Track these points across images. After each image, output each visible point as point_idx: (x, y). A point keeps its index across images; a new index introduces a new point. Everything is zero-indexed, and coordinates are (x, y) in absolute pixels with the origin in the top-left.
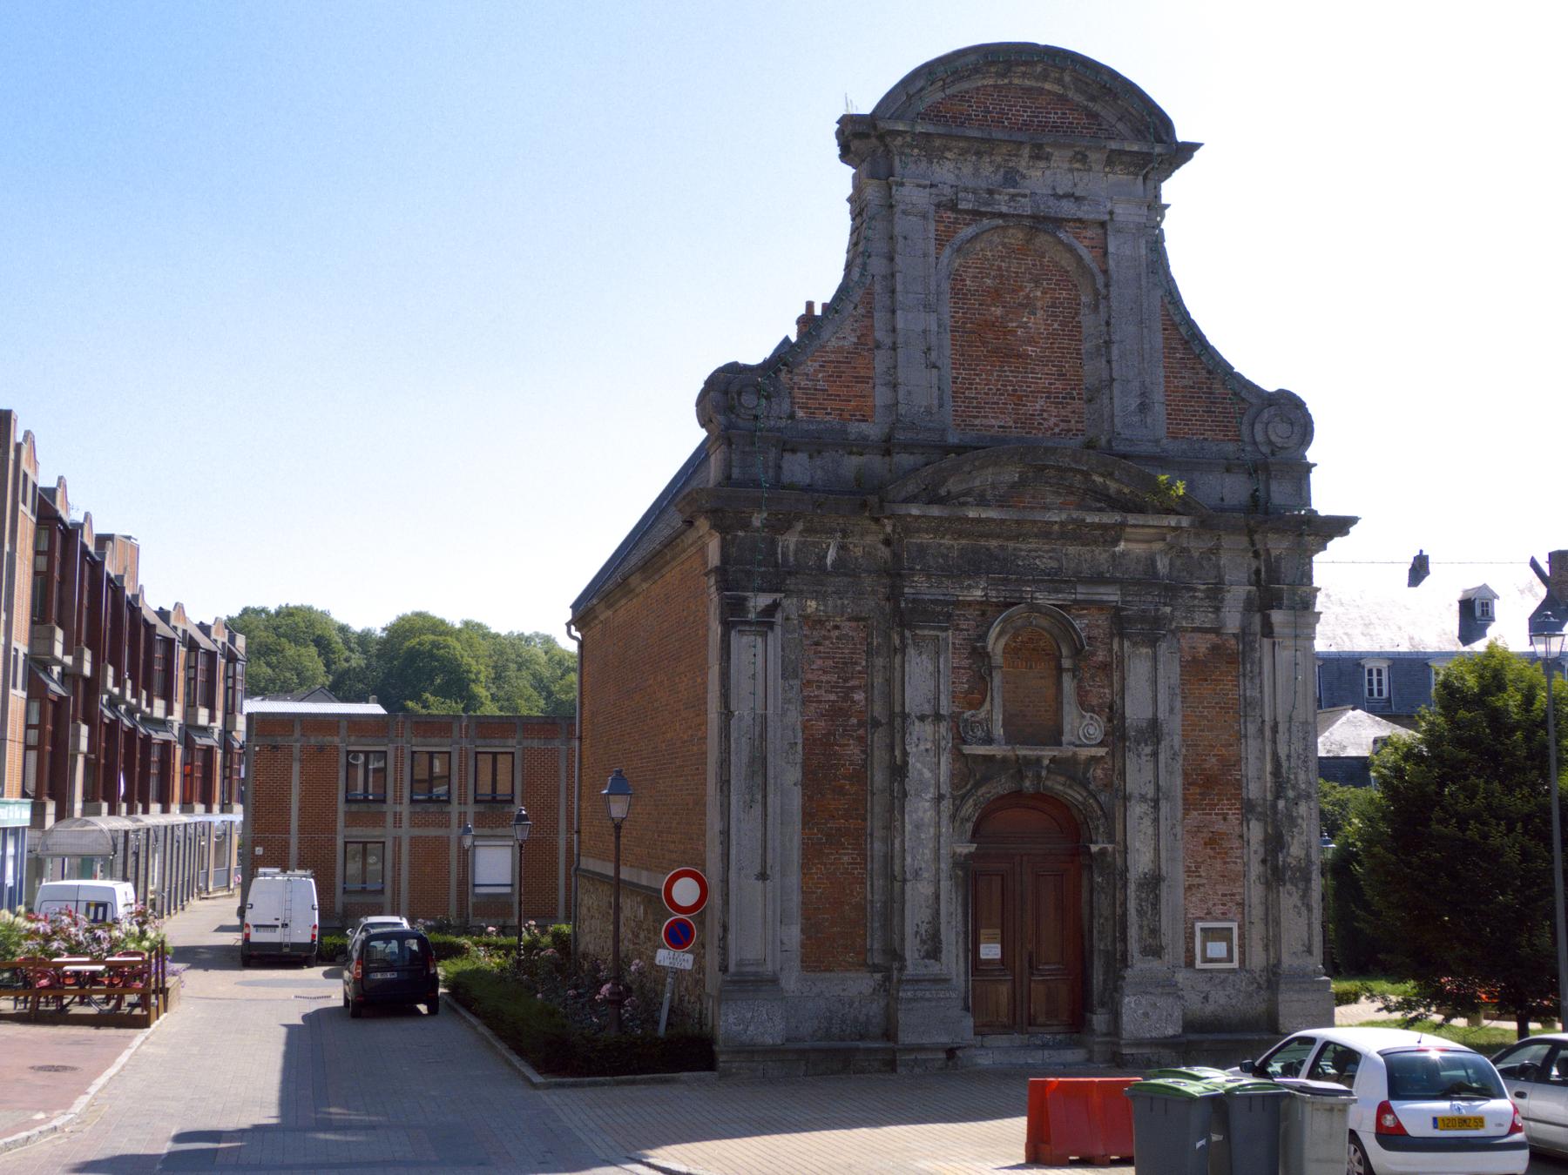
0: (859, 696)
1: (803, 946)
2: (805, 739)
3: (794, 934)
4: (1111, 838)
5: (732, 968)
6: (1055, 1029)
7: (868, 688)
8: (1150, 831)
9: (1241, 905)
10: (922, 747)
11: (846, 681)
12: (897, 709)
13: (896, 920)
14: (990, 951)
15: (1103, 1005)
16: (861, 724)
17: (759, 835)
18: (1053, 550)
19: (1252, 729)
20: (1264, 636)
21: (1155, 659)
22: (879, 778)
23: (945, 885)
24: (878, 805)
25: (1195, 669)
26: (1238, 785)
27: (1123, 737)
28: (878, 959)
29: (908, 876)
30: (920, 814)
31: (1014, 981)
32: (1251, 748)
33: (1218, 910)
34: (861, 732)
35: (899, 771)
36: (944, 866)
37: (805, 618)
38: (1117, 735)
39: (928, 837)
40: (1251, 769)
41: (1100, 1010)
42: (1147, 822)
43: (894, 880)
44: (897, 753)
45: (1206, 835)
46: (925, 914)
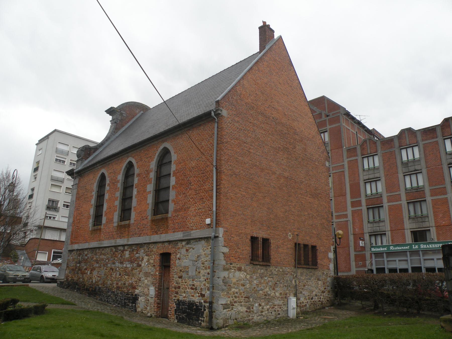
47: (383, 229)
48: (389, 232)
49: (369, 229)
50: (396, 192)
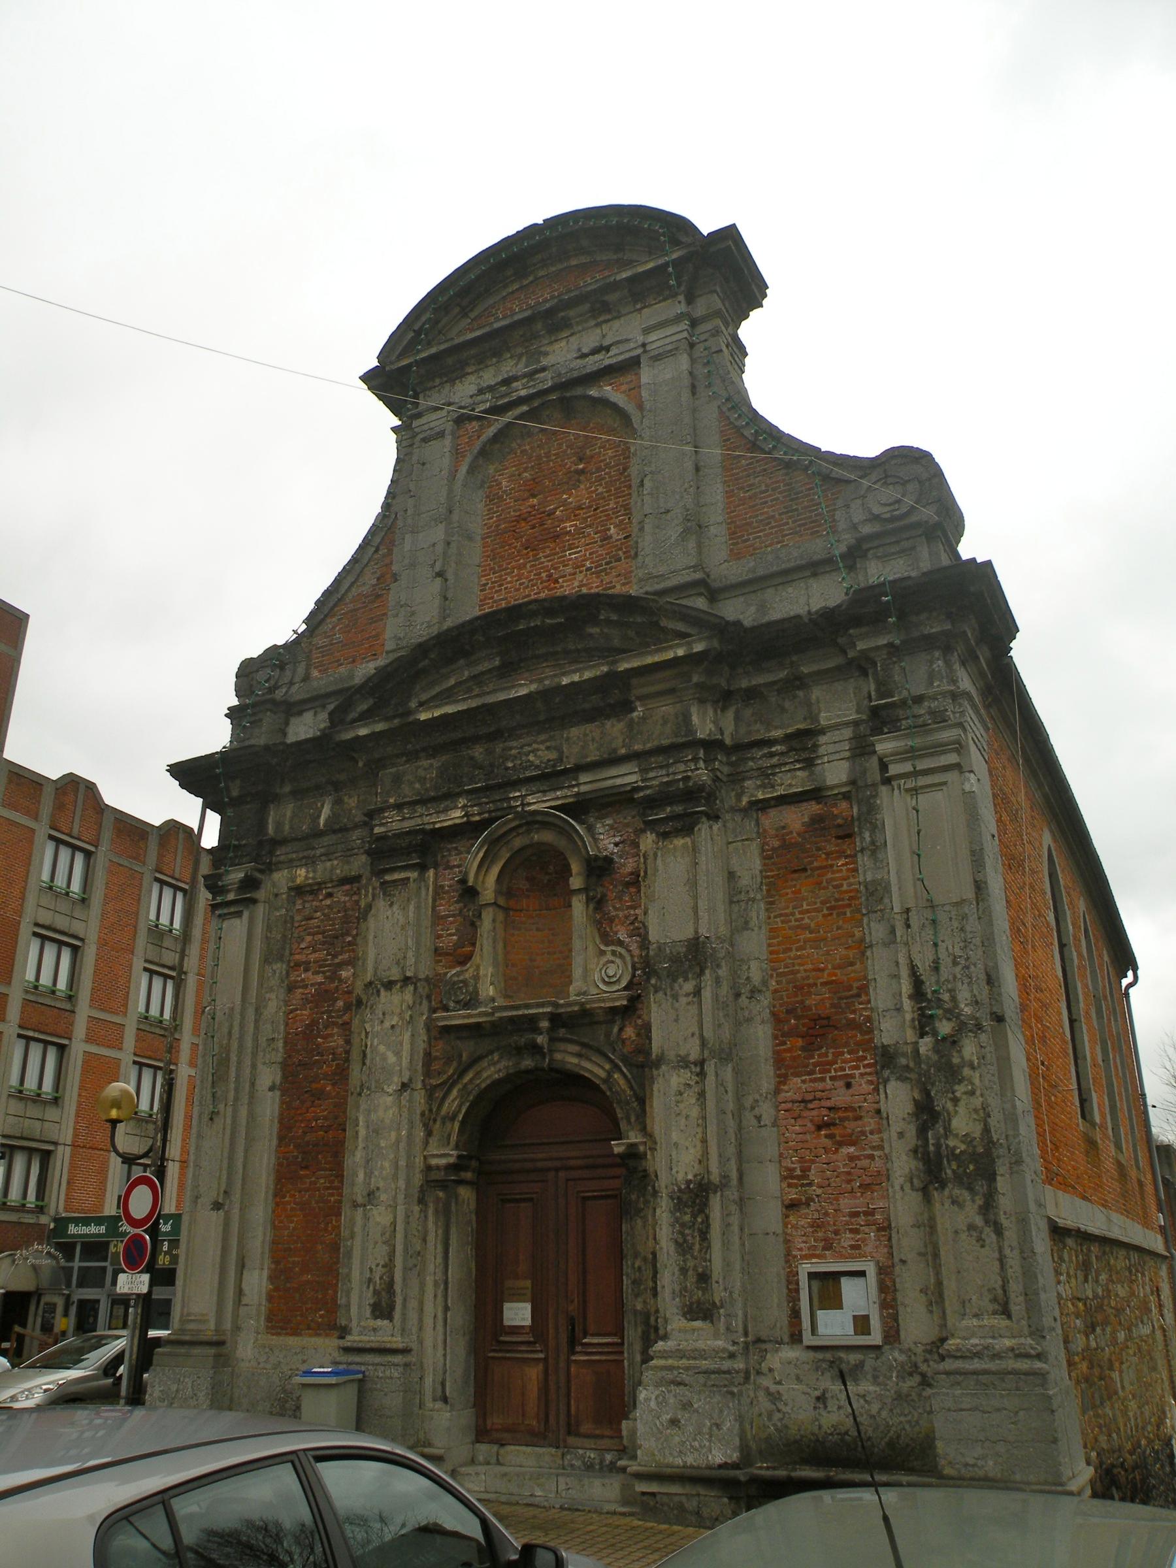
4: (644, 1130)
8: (695, 1112)
10: (387, 1024)
11: (335, 956)
14: (519, 1314)
18: (551, 738)
21: (695, 850)
25: (787, 864)
26: (867, 1028)
30: (381, 1113)
32: (879, 965)
33: (847, 1240)
40: (881, 997)
42: (690, 1098)
45: (816, 1113)
46: (379, 1254)
47: (52, 1132)
48: (68, 1149)
49: (11, 1120)
50: (116, 1013)
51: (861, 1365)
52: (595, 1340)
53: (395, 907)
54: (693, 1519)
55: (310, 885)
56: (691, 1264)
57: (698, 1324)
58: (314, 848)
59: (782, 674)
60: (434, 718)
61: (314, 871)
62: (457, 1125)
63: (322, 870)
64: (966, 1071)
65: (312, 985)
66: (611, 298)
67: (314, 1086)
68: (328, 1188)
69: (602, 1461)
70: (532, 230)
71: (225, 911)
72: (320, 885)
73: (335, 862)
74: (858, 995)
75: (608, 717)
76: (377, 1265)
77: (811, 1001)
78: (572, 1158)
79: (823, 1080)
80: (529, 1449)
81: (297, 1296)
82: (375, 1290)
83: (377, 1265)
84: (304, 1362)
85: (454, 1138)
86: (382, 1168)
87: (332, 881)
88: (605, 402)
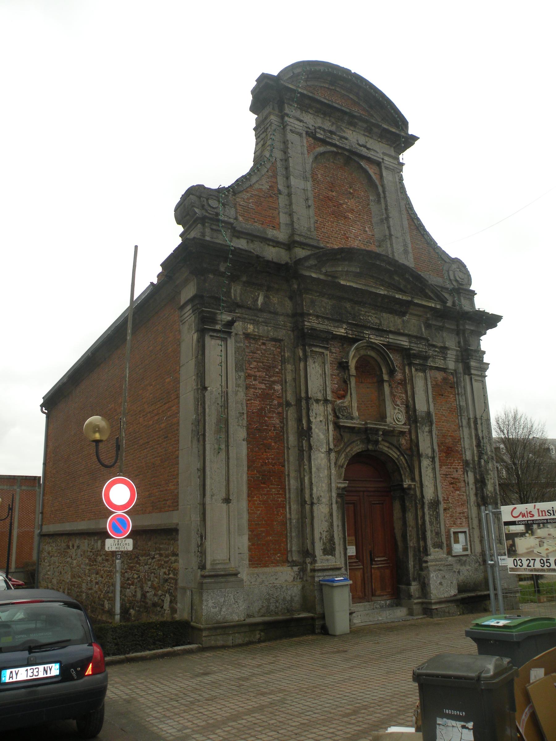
0: (278, 387)
1: (250, 550)
2: (248, 412)
3: (243, 542)
5: (208, 566)
6: (385, 597)
7: (283, 382)
8: (431, 475)
9: (467, 518)
10: (318, 419)
11: (270, 377)
12: (303, 395)
13: (308, 530)
15: (414, 580)
16: (280, 405)
17: (224, 472)
18: (376, 314)
19: (465, 422)
20: (465, 374)
22: (292, 439)
23: (335, 506)
24: (292, 456)
27: (416, 421)
28: (295, 557)
29: (315, 501)
30: (319, 461)
31: (363, 569)
34: (280, 410)
35: (305, 433)
36: (334, 495)
37: (247, 336)
38: (412, 417)
39: (324, 475)
40: (466, 443)
41: (413, 583)
43: (306, 504)
44: (304, 422)
51: (466, 561)
52: (379, 559)
53: (316, 364)
54: (447, 614)
55: (255, 335)
56: (433, 529)
57: (437, 549)
58: (258, 317)
59: (441, 324)
60: (346, 285)
61: (258, 329)
62: (344, 470)
63: (262, 330)
64: (490, 472)
65: (259, 389)
66: (375, 130)
67: (265, 442)
68: (277, 494)
69: (386, 604)
70: (348, 71)
71: (215, 334)
72: (260, 337)
73: (270, 328)
74: (458, 442)
75: (397, 315)
76: (324, 531)
77: (447, 441)
78: (360, 487)
79: (450, 468)
80: (361, 604)
81: (265, 548)
82: (323, 543)
83: (324, 531)
84: (276, 579)
85: (343, 475)
86: (322, 487)
87: (268, 337)
88: (366, 172)
